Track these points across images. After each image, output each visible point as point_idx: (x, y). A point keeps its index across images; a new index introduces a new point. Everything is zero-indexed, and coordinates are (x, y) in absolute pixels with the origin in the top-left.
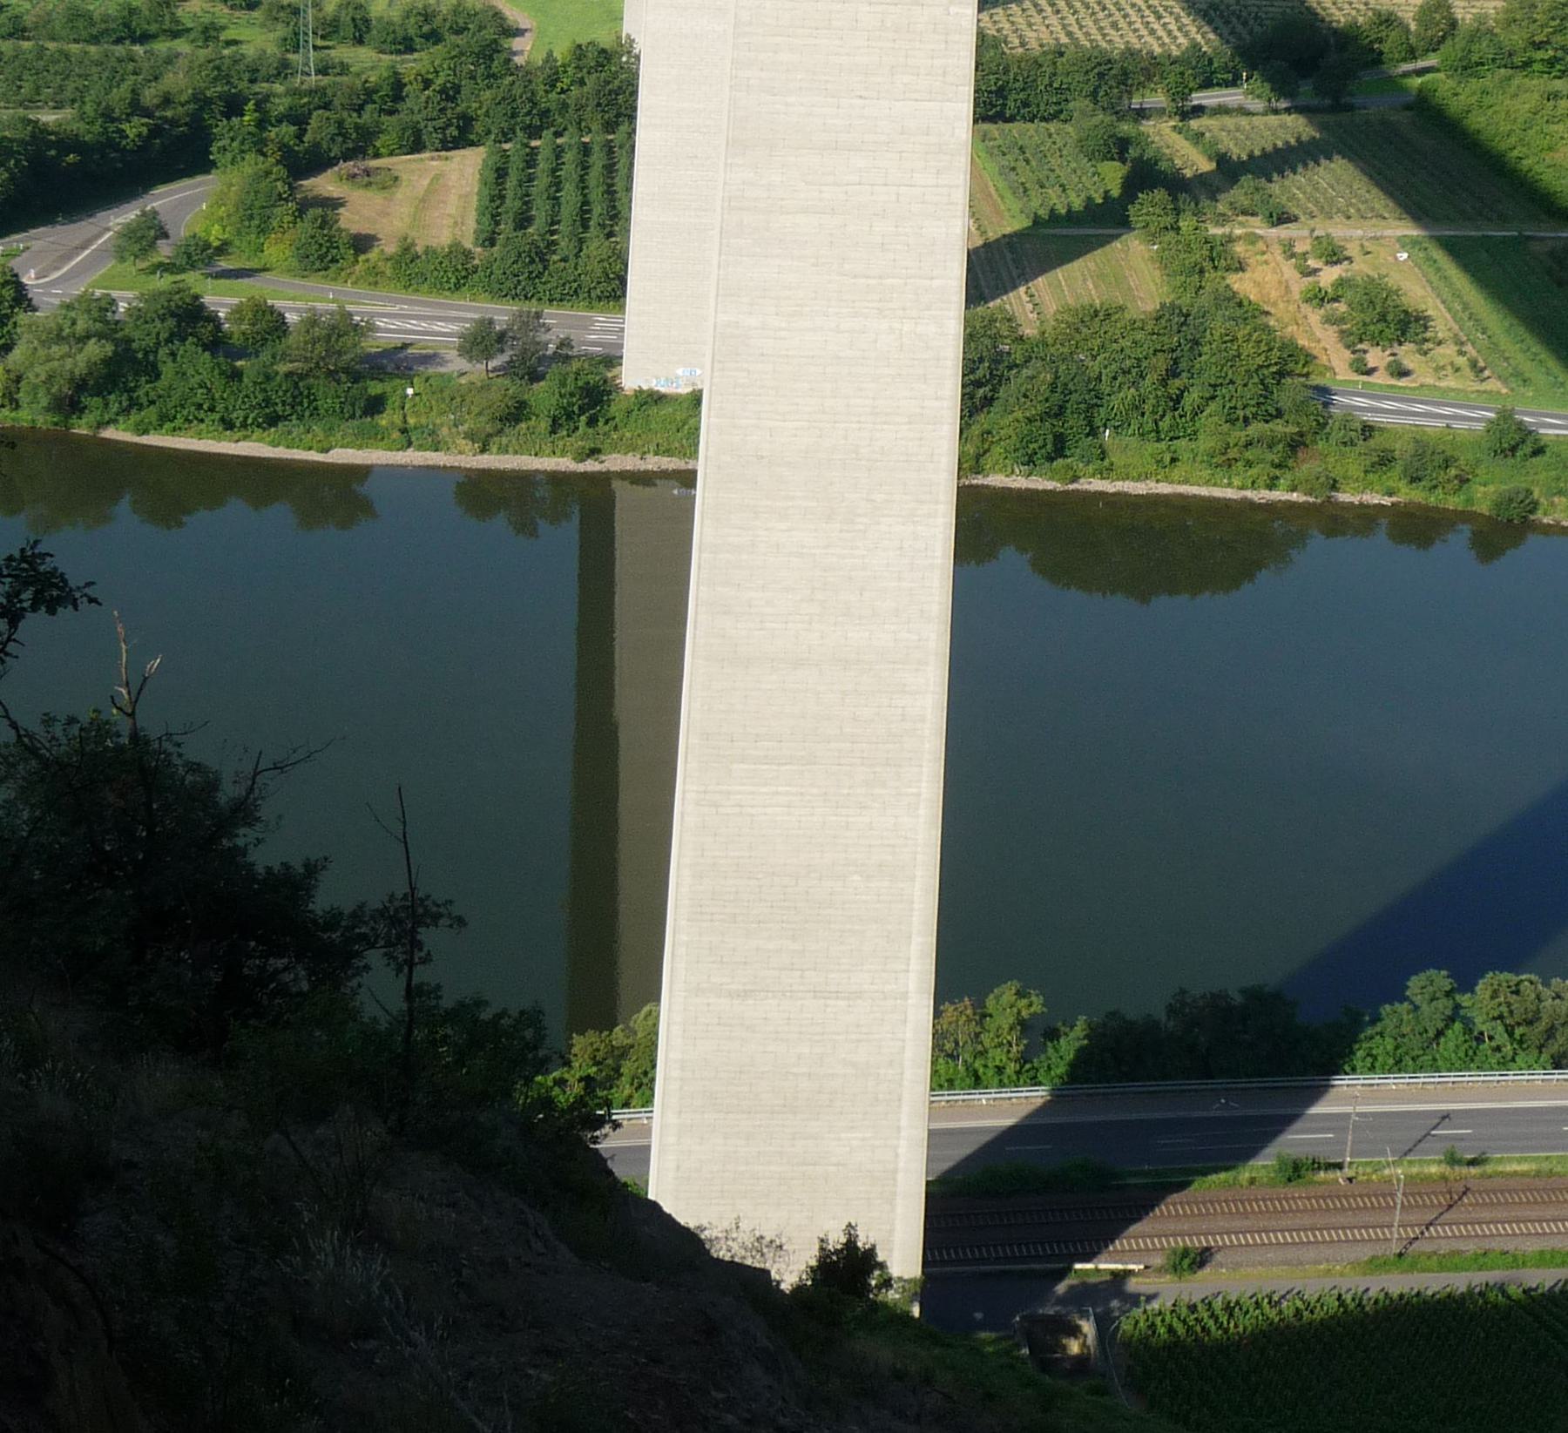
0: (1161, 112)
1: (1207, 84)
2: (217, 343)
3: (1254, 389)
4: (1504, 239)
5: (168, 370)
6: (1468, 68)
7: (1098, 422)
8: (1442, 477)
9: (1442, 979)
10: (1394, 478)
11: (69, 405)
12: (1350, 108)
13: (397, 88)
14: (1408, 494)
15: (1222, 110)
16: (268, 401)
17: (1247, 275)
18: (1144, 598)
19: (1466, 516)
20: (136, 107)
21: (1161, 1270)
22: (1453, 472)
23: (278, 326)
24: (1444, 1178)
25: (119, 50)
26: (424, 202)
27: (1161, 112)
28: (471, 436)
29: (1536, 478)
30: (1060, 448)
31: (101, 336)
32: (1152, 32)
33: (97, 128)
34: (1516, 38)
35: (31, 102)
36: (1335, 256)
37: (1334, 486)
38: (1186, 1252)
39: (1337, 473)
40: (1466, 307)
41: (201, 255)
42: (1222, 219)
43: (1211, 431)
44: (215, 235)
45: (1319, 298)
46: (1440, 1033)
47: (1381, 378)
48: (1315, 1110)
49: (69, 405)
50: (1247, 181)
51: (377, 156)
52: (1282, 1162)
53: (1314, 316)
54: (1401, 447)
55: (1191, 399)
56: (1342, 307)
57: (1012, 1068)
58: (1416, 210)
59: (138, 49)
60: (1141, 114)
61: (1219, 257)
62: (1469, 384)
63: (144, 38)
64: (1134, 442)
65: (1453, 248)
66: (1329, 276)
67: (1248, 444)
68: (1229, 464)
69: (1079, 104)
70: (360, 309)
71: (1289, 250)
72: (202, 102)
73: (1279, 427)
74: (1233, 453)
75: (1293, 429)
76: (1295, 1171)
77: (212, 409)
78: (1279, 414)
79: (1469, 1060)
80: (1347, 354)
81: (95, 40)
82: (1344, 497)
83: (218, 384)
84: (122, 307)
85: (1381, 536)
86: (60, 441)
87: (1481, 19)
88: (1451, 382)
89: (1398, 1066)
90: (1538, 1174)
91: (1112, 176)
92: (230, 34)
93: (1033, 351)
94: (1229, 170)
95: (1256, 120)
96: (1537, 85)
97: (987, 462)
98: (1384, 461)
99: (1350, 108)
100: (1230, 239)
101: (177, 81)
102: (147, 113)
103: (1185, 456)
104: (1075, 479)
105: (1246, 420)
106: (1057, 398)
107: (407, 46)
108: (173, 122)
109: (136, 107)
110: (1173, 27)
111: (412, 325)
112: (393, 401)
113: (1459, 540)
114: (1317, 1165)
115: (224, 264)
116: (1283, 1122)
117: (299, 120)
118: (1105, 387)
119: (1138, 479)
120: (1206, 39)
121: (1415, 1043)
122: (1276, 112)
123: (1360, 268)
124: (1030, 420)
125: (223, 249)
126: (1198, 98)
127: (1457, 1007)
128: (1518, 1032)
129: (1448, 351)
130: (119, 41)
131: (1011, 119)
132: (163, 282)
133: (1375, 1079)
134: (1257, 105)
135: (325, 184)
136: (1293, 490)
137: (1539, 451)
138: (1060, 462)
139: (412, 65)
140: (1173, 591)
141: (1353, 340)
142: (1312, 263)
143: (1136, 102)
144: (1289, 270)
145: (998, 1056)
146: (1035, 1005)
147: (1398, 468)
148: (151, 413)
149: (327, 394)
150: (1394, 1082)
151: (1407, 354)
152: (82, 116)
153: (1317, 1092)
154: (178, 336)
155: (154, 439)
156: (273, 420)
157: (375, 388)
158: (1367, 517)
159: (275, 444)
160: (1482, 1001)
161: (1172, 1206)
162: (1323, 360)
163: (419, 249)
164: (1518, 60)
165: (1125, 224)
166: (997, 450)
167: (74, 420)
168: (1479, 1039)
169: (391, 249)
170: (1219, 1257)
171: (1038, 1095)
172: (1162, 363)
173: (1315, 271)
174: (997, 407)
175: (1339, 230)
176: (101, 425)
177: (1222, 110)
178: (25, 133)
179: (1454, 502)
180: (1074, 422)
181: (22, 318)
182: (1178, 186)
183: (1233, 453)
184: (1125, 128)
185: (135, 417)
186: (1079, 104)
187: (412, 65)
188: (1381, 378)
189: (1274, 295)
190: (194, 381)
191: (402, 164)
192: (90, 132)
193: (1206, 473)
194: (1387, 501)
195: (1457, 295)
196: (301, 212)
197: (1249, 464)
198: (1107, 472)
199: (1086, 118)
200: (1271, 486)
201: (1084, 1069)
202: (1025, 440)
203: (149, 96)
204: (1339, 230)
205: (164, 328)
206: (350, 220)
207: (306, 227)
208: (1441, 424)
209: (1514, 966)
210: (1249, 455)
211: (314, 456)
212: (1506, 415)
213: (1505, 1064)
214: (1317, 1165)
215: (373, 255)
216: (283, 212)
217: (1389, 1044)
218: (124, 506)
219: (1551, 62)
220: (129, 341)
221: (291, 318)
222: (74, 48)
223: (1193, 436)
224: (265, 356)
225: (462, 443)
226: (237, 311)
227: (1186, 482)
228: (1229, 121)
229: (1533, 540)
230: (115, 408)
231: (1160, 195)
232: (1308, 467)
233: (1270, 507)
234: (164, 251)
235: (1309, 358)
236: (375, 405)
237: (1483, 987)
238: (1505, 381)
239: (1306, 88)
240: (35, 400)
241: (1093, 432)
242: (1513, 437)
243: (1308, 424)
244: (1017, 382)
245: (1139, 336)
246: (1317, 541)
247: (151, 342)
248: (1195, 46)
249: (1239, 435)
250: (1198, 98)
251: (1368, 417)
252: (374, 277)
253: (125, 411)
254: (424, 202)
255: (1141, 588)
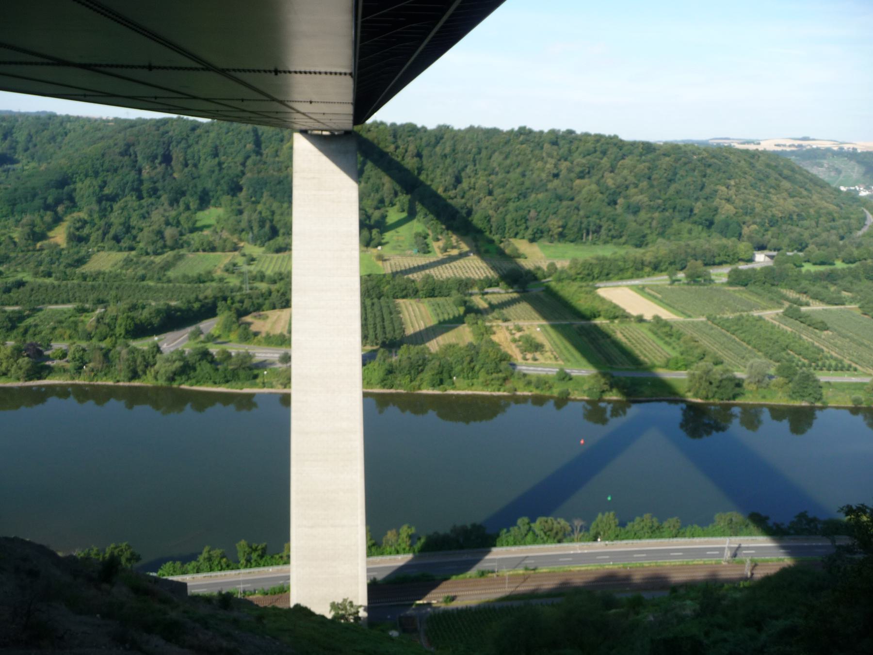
0: (476, 294)
1: (490, 286)
2: (213, 361)
3: (493, 365)
4: (566, 325)
5: (199, 369)
6: (560, 280)
7: (452, 375)
8: (544, 387)
9: (526, 520)
10: (532, 388)
11: (172, 379)
12: (527, 291)
13: (270, 293)
14: (536, 392)
15: (493, 293)
16: (225, 377)
17: (496, 335)
18: (468, 422)
19: (551, 397)
20: (197, 299)
21: (441, 602)
22: (547, 385)
23: (229, 356)
24: (524, 574)
25: (196, 285)
26: (275, 323)
27: (476, 294)
28: (282, 384)
29: (569, 386)
30: (441, 382)
31: (180, 360)
32: (477, 273)
33: (186, 305)
34: (572, 272)
35: (171, 299)
36: (520, 329)
37: (516, 390)
38: (448, 597)
39: (517, 387)
40: (554, 342)
41: (212, 339)
42: (490, 321)
43: (482, 375)
44: (217, 333)
45: (515, 341)
46: (526, 535)
47: (530, 361)
48: (488, 557)
49: (172, 379)
50: (497, 310)
51: (263, 311)
52: (479, 571)
53: (513, 346)
54: (534, 379)
55: (477, 368)
56: (520, 343)
57: (407, 548)
58: (545, 317)
59: (202, 285)
60: (471, 294)
61: (489, 331)
62: (554, 362)
63: (204, 282)
64: (462, 380)
65: (553, 326)
66: (518, 335)
67: (492, 380)
68: (487, 385)
69: (454, 292)
70: (251, 351)
71: (507, 328)
72: (216, 298)
73: (500, 375)
74: (488, 382)
75: (504, 375)
76: (482, 574)
77: (211, 379)
78: (501, 371)
79: (535, 541)
80: (522, 355)
81: (189, 283)
82: (519, 393)
83: (212, 372)
84: (187, 353)
85: (529, 404)
86: (170, 390)
87: (563, 267)
88: (549, 362)
89: (515, 544)
90: (550, 572)
91: (462, 310)
92: (227, 280)
93: (435, 356)
94: (492, 307)
95: (503, 295)
96: (577, 284)
97: (422, 387)
98: (529, 383)
99: (527, 291)
100: (491, 327)
101: (209, 293)
102: (200, 301)
103: (475, 383)
104: (446, 390)
105: (492, 373)
106: (440, 369)
107: (275, 282)
108: (208, 303)
109: (197, 299)
110: (482, 272)
111: (268, 355)
112: (261, 375)
113: (551, 403)
114: (489, 572)
115: (219, 340)
116: (477, 561)
117: (242, 301)
118: (453, 366)
119: (463, 390)
120: (492, 274)
121: (520, 537)
122: (508, 293)
123: (527, 332)
124: (433, 375)
125: (219, 337)
126: (486, 290)
127: (530, 527)
128: (548, 533)
129: (549, 354)
130: (196, 283)
131: (436, 297)
132: (199, 346)
133: (508, 548)
134: (502, 291)
135: (248, 319)
136: (505, 391)
137: (571, 379)
138: (441, 386)
139: (274, 287)
140: (475, 420)
141: (524, 351)
142: (513, 332)
143: (470, 291)
144: (507, 334)
145: (403, 545)
146: (413, 530)
147: (533, 384)
148: (194, 381)
149: (242, 373)
150: (514, 549)
151: (538, 355)
152: (182, 302)
153: (488, 552)
154: (201, 359)
155: (196, 388)
156: (227, 381)
157: (256, 372)
158: (525, 399)
159: (228, 388)
160: (537, 526)
161: (444, 585)
162: (515, 357)
163: (271, 335)
164: (573, 278)
165: (463, 323)
166: (425, 383)
167: (173, 383)
168: (537, 536)
169: (264, 335)
170: (458, 598)
171: (408, 557)
172: (468, 359)
173: (514, 334)
174: (425, 371)
175: (521, 323)
176: (180, 384)
177: (493, 293)
178: (165, 307)
179: (547, 393)
180: (445, 375)
181: (158, 356)
182: (478, 312)
183: (488, 382)
184: (467, 298)
185: (189, 382)
186: (454, 292)
187: (274, 287)
188: (530, 361)
189: (503, 340)
190: (205, 372)
191: (270, 313)
192: (184, 307)
193: (481, 388)
194: (530, 394)
195: (552, 339)
196: (240, 325)
197: (493, 385)
198: (454, 388)
199: (455, 296)
200: (499, 390)
201: (424, 549)
202: (432, 380)
203: (201, 297)
204: (521, 323)
205: (198, 357)
206: (253, 328)
207: (241, 330)
208: (544, 373)
209: (547, 514)
210: (493, 382)
211: (238, 391)
212: (562, 370)
213: (544, 542)
214: (489, 572)
215: (259, 337)
216: (235, 326)
217: (512, 538)
218: (188, 406)
219: (582, 278)
220: (188, 361)
221: (233, 354)
222: (184, 285)
223: (478, 378)
224: (225, 364)
225: (280, 386)
226: (218, 353)
227: (476, 390)
228: (495, 296)
229: (570, 403)
230: (184, 379)
231: (473, 315)
232: (509, 385)
233: (499, 397)
234: (202, 337)
235: (511, 357)
236: (256, 377)
237: (538, 522)
238: (563, 361)
239: (516, 287)
240: (162, 378)
241: (451, 378)
242: (564, 375)
243: (508, 374)
244: (430, 365)
245: (462, 351)
246: (513, 405)
247: (194, 361)
248: (487, 277)
249: (490, 377)
250: (486, 290)
251: (526, 372)
252: (259, 343)
253: (187, 380)
254: (275, 323)
255: (467, 419)
